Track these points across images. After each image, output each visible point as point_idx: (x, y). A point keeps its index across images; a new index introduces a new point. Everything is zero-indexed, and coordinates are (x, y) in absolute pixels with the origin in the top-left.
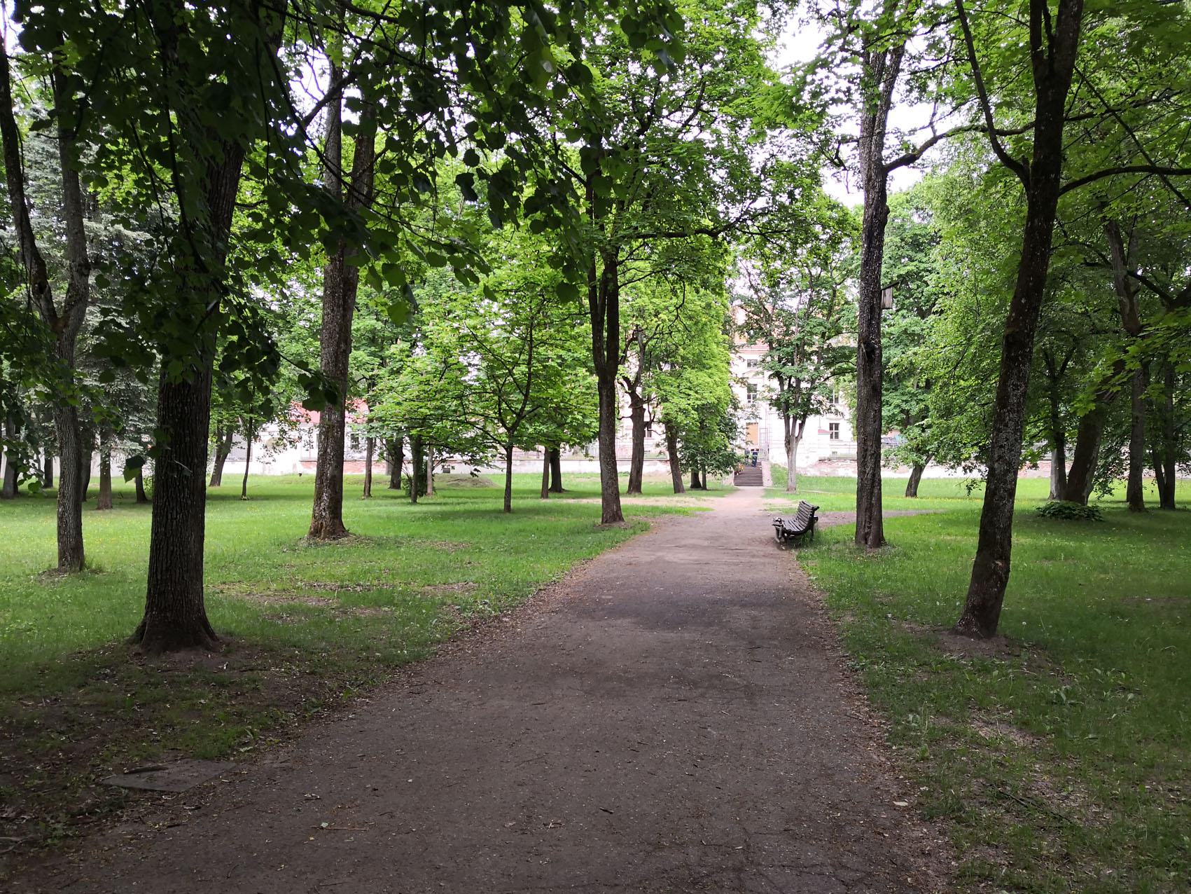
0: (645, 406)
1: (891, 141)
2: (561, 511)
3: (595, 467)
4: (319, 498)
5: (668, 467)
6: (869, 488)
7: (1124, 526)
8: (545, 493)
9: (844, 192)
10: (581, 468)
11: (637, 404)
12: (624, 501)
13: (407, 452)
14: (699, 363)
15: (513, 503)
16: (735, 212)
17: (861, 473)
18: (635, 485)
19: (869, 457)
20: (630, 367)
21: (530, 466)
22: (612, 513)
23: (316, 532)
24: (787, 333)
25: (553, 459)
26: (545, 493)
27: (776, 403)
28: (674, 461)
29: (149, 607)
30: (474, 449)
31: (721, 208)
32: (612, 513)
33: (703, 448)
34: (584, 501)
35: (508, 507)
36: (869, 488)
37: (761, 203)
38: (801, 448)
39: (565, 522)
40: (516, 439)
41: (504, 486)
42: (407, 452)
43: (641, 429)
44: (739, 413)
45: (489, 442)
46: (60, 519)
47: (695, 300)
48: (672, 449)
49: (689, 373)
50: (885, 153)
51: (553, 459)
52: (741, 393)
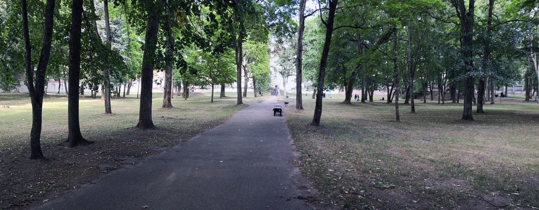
0: (114, 46)
1: (306, 9)
2: (226, 102)
3: (236, 90)
4: (165, 97)
5: (253, 90)
6: (299, 95)
7: (360, 106)
8: (221, 97)
9: (296, 19)
10: (231, 90)
11: (246, 73)
12: (243, 99)
13: (182, 86)
14: (262, 62)
15: (214, 100)
16: (271, 23)
17: (297, 91)
18: (245, 95)
19: (299, 88)
20: (244, 63)
21: (218, 89)
22: (240, 102)
23: (164, 106)
24: (284, 54)
25: (223, 89)
26: (221, 97)
27: (281, 73)
28: (255, 88)
29: (140, 119)
30: (203, 85)
31: (267, 22)
32: (240, 102)
33: (261, 83)
34: (230, 99)
35: (212, 101)
36: (299, 95)
37: (277, 21)
38: (287, 85)
39: (226, 105)
40: (215, 82)
41: (211, 95)
42: (182, 86)
43: (247, 80)
44: (272, 76)
45: (207, 83)
46: (106, 101)
47: (261, 45)
48: (254, 85)
49: (259, 64)
50: (305, 12)
51: (223, 89)
52: (272, 70)
